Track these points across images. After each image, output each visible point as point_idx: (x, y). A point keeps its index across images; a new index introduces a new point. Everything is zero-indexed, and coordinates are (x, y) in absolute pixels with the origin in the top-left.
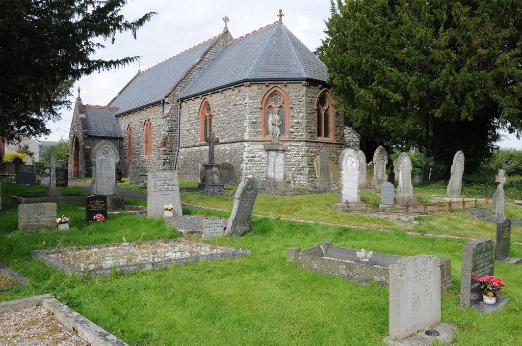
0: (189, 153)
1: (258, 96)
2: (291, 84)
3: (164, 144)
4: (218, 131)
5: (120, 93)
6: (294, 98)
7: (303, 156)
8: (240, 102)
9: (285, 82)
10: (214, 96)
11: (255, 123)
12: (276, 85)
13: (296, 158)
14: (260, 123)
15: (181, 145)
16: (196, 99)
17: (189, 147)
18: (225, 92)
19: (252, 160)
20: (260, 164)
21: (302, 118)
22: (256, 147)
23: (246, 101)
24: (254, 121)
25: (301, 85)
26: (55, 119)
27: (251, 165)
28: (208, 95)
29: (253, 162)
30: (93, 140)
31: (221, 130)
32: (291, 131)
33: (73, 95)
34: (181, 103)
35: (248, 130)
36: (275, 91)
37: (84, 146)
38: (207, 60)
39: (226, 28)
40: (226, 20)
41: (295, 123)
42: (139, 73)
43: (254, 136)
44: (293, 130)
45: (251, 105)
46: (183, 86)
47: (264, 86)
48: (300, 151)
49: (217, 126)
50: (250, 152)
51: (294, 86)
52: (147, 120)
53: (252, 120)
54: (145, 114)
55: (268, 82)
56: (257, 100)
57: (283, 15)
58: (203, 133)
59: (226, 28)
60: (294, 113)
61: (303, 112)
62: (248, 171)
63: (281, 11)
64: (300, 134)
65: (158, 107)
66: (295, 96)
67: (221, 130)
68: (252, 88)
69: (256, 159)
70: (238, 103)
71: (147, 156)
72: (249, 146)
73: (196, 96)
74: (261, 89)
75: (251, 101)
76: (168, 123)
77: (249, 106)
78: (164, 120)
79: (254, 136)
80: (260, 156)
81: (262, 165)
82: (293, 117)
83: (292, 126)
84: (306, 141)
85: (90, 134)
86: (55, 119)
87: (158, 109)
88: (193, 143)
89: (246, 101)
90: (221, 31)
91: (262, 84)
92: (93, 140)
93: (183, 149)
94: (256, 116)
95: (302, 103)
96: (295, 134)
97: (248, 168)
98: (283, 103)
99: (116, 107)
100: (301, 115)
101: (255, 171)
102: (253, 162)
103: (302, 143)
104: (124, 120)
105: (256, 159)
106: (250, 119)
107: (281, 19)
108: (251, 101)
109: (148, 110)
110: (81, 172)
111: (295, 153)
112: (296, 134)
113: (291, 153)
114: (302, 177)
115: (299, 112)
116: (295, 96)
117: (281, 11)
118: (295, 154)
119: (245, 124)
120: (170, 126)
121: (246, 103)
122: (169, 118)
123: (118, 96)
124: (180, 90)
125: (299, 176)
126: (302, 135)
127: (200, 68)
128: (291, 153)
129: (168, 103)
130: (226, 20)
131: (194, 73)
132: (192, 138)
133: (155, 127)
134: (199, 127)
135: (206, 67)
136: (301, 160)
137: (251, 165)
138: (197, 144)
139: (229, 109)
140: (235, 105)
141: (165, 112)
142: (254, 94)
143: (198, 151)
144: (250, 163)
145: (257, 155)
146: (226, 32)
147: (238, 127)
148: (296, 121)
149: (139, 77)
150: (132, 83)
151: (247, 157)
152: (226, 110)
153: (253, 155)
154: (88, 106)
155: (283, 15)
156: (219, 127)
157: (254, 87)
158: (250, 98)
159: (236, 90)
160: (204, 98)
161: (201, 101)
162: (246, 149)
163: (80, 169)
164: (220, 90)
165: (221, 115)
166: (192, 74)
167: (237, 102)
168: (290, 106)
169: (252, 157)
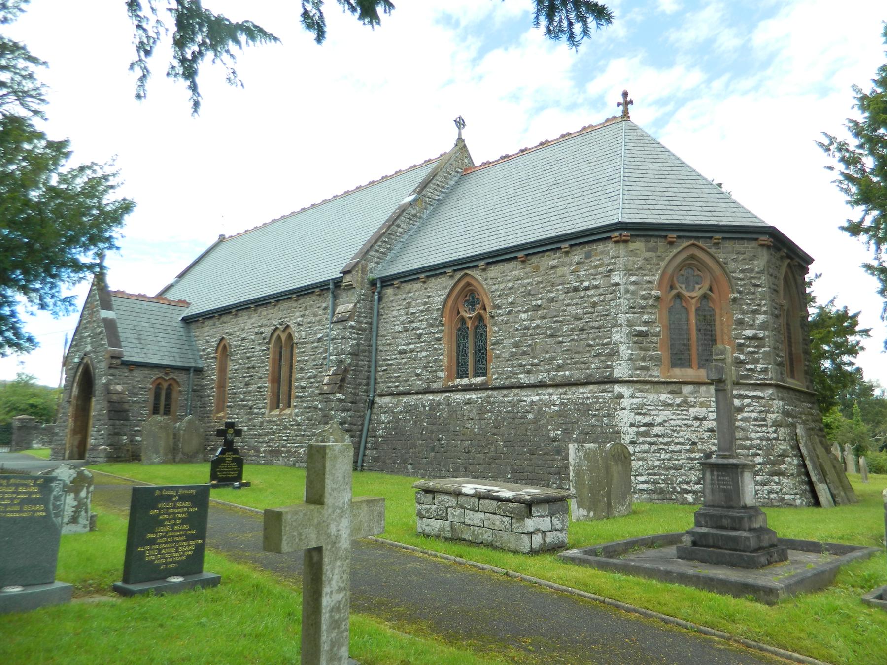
0: (411, 409)
1: (649, 267)
2: (732, 242)
3: (341, 382)
4: (513, 355)
5: (181, 276)
6: (741, 276)
7: (777, 424)
8: (595, 283)
9: (719, 236)
10: (493, 271)
11: (641, 334)
12: (692, 242)
13: (759, 429)
14: (657, 335)
15: (382, 388)
16: (433, 280)
17: (408, 393)
18: (535, 260)
19: (646, 434)
20: (667, 444)
21: (763, 327)
22: (651, 397)
23: (616, 278)
24: (644, 329)
25: (754, 244)
26: (57, 309)
27: (646, 447)
28: (477, 266)
29: (648, 439)
30: (131, 370)
31: (524, 353)
32: (737, 358)
33: (118, 248)
34: (382, 287)
35: (625, 351)
36: (692, 257)
37: (107, 385)
38: (428, 200)
39: (460, 140)
40: (460, 123)
41: (748, 338)
42: (222, 239)
43: (642, 368)
44: (742, 357)
45: (632, 288)
46: (382, 250)
47: (661, 243)
48: (768, 412)
49: (507, 342)
50: (638, 410)
51: (738, 246)
52: (281, 328)
53: (638, 328)
54: (273, 317)
55: (675, 235)
56: (648, 278)
57: (631, 102)
58: (454, 359)
59: (460, 140)
60: (743, 313)
61: (765, 313)
62: (640, 463)
63: (625, 94)
64: (761, 366)
65: (314, 298)
66: (742, 271)
67: (524, 353)
68: (632, 246)
69: (656, 430)
70: (586, 284)
71: (277, 412)
72: (632, 397)
73: (434, 271)
74: (654, 250)
75: (633, 279)
76: (351, 333)
77: (627, 291)
78: (340, 326)
79: (642, 368)
80: (665, 421)
81: (673, 447)
82: (740, 322)
83: (741, 345)
84: (777, 386)
85: (125, 358)
86: (57, 309)
87: (319, 305)
88: (420, 384)
89: (616, 278)
90: (448, 145)
91: (660, 237)
92: (131, 370)
93: (386, 399)
94: (646, 317)
95: (760, 289)
96: (748, 367)
97: (639, 455)
98: (711, 289)
99: (184, 302)
100: (761, 318)
101: (657, 463)
102: (648, 439)
103: (770, 391)
104: (206, 329)
105: (656, 430)
106: (630, 324)
107: (626, 113)
108: (633, 279)
109: (284, 305)
110: (95, 448)
111: (754, 415)
112: (753, 367)
113: (745, 415)
114: (785, 480)
115: (755, 312)
116: (742, 271)
117: (625, 94)
118: (755, 420)
119: (616, 337)
120: (355, 342)
121: (617, 284)
122: (353, 323)
123: (177, 282)
124: (376, 260)
125: (776, 479)
126: (765, 371)
127: (414, 216)
128: (745, 415)
129: (350, 287)
130: (460, 123)
131: (403, 226)
132: (418, 371)
133: (301, 343)
134: (444, 346)
135: (426, 213)
136: (775, 436)
137: (646, 447)
138: (434, 386)
139: (552, 300)
140: (576, 289)
141: (340, 309)
142: (640, 262)
143: (439, 404)
144: (641, 439)
145: (659, 420)
146: (461, 146)
147: (590, 346)
148: (748, 333)
149: (223, 246)
150: (213, 255)
151: (632, 425)
152: (539, 302)
153: (647, 419)
154: (119, 294)
155: (631, 102)
156: (516, 345)
157: (638, 245)
158: (629, 272)
159: (577, 256)
160: (459, 275)
161: (452, 283)
162: (625, 402)
163: (91, 441)
164: (520, 254)
165: (523, 316)
166: (399, 226)
167: (582, 282)
168: (732, 295)
169: (645, 425)
